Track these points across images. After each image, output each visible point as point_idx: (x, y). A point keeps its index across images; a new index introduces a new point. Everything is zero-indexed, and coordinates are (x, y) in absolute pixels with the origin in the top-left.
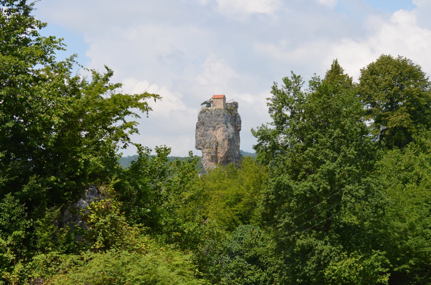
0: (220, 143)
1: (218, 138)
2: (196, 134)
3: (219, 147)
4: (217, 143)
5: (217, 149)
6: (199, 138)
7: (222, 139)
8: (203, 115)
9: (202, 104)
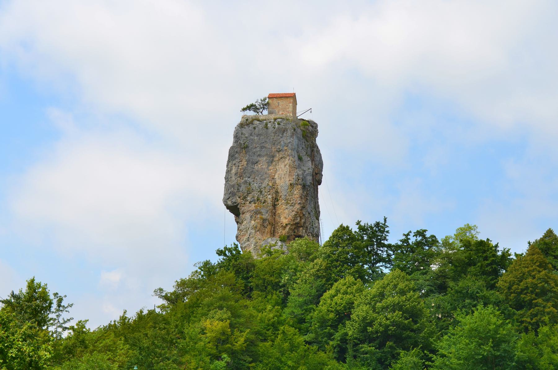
2: (228, 172)
4: (277, 192)
6: (234, 180)
7: (288, 183)
8: (246, 131)
9: (244, 110)
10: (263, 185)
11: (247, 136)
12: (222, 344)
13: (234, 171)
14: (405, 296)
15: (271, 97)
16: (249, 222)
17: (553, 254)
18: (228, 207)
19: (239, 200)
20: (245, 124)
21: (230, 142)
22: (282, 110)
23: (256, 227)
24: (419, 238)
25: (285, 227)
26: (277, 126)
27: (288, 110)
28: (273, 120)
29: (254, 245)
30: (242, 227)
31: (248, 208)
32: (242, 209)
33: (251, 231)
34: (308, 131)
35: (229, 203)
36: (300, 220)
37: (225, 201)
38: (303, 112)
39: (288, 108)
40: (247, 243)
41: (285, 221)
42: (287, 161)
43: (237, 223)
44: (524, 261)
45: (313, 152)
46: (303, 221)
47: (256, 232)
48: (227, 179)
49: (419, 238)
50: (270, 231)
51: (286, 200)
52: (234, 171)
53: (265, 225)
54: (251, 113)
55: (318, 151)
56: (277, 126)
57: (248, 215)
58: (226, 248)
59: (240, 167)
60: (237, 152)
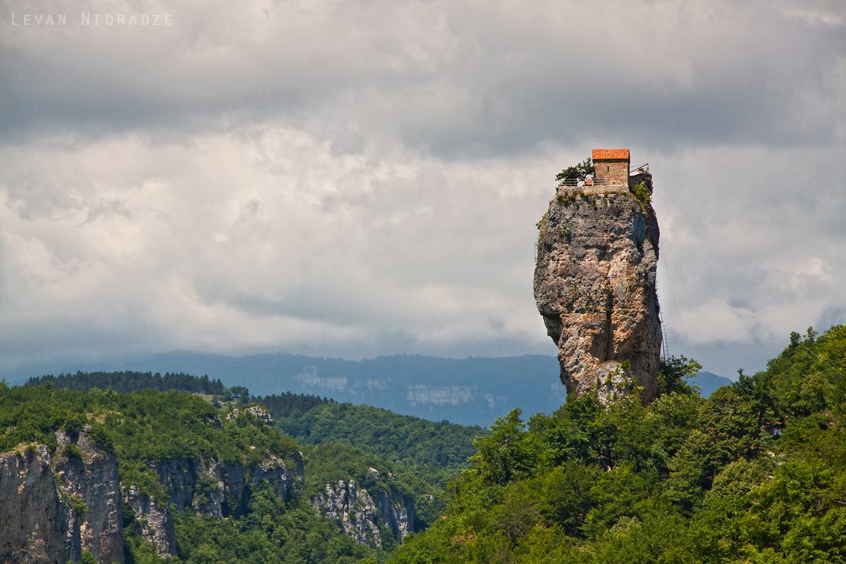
7: (626, 284)
10: (594, 288)
11: (568, 217)
12: (753, 389)
14: (101, 390)
19: (561, 308)
23: (587, 346)
26: (609, 204)
27: (621, 178)
28: (603, 196)
29: (585, 370)
33: (580, 350)
36: (643, 333)
39: (622, 175)
40: (575, 367)
42: (624, 254)
44: (214, 525)
46: (645, 333)
47: (586, 352)
50: (604, 349)
53: (598, 342)
56: (609, 204)
57: (574, 329)
59: (560, 262)
60: (555, 241)
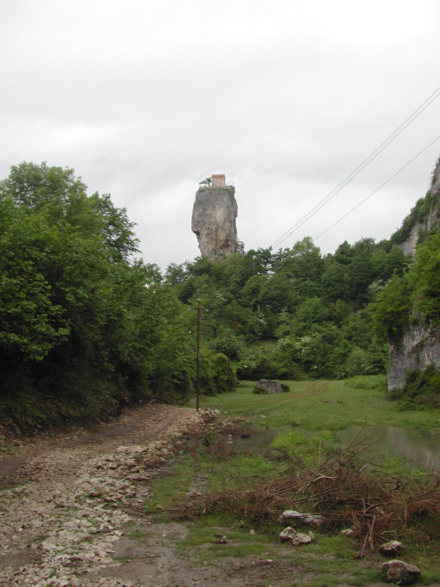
0: (220, 225)
1: (218, 219)
2: (193, 215)
3: (219, 230)
4: (217, 225)
5: (216, 231)
6: (197, 219)
8: (203, 194)
9: (200, 183)
13: (196, 214)
15: (213, 176)
16: (204, 239)
17: (109, 544)
18: (194, 232)
20: (201, 191)
21: (194, 200)
22: (218, 183)
24: (287, 252)
25: (221, 241)
30: (201, 242)
31: (204, 232)
32: (201, 233)
34: (230, 191)
35: (195, 230)
37: (192, 229)
38: (228, 182)
41: (222, 239)
42: (222, 209)
43: (198, 238)
45: (233, 201)
48: (193, 218)
49: (287, 252)
51: (222, 228)
52: (196, 214)
54: (203, 185)
55: (235, 201)
57: (204, 236)
58: (198, 257)
